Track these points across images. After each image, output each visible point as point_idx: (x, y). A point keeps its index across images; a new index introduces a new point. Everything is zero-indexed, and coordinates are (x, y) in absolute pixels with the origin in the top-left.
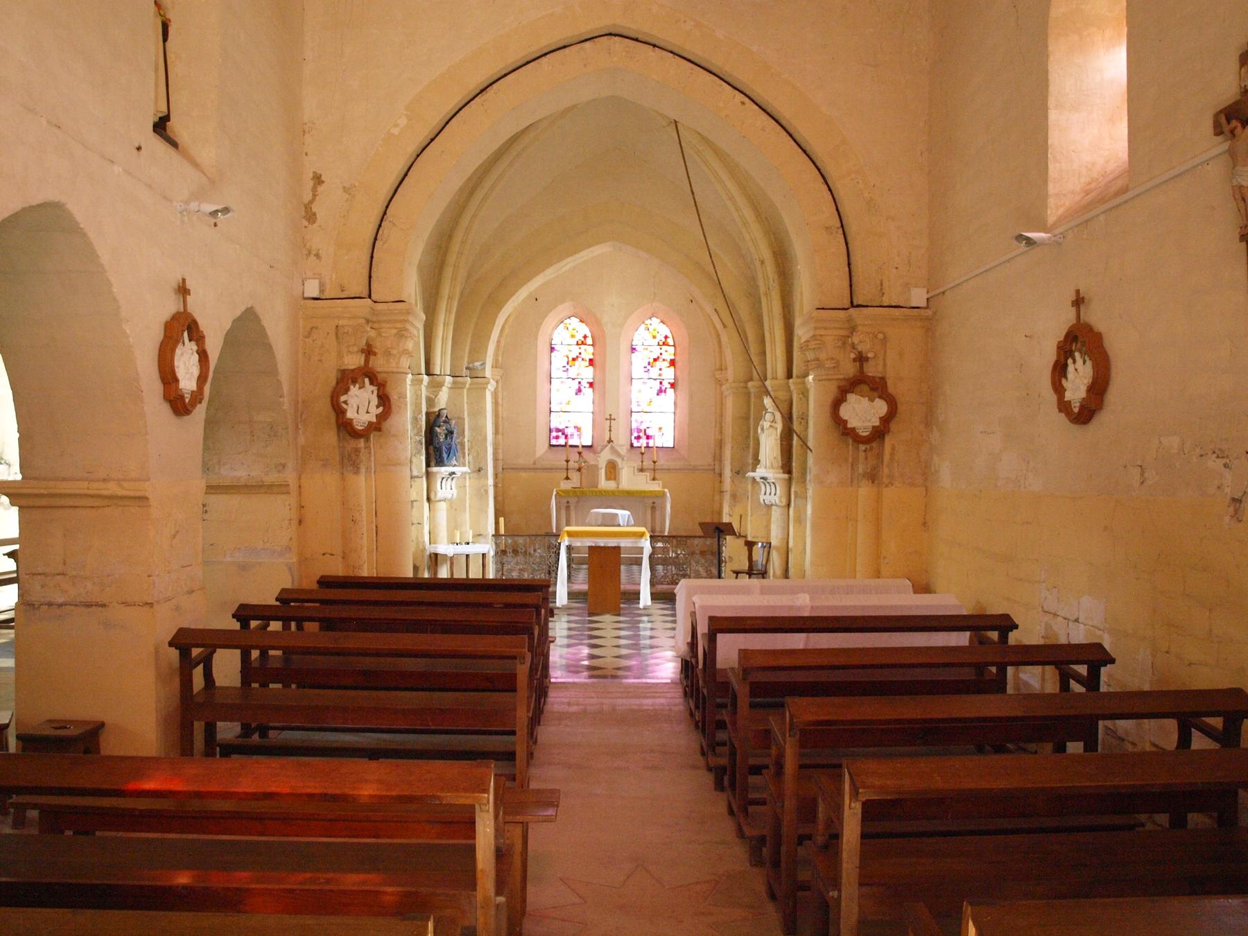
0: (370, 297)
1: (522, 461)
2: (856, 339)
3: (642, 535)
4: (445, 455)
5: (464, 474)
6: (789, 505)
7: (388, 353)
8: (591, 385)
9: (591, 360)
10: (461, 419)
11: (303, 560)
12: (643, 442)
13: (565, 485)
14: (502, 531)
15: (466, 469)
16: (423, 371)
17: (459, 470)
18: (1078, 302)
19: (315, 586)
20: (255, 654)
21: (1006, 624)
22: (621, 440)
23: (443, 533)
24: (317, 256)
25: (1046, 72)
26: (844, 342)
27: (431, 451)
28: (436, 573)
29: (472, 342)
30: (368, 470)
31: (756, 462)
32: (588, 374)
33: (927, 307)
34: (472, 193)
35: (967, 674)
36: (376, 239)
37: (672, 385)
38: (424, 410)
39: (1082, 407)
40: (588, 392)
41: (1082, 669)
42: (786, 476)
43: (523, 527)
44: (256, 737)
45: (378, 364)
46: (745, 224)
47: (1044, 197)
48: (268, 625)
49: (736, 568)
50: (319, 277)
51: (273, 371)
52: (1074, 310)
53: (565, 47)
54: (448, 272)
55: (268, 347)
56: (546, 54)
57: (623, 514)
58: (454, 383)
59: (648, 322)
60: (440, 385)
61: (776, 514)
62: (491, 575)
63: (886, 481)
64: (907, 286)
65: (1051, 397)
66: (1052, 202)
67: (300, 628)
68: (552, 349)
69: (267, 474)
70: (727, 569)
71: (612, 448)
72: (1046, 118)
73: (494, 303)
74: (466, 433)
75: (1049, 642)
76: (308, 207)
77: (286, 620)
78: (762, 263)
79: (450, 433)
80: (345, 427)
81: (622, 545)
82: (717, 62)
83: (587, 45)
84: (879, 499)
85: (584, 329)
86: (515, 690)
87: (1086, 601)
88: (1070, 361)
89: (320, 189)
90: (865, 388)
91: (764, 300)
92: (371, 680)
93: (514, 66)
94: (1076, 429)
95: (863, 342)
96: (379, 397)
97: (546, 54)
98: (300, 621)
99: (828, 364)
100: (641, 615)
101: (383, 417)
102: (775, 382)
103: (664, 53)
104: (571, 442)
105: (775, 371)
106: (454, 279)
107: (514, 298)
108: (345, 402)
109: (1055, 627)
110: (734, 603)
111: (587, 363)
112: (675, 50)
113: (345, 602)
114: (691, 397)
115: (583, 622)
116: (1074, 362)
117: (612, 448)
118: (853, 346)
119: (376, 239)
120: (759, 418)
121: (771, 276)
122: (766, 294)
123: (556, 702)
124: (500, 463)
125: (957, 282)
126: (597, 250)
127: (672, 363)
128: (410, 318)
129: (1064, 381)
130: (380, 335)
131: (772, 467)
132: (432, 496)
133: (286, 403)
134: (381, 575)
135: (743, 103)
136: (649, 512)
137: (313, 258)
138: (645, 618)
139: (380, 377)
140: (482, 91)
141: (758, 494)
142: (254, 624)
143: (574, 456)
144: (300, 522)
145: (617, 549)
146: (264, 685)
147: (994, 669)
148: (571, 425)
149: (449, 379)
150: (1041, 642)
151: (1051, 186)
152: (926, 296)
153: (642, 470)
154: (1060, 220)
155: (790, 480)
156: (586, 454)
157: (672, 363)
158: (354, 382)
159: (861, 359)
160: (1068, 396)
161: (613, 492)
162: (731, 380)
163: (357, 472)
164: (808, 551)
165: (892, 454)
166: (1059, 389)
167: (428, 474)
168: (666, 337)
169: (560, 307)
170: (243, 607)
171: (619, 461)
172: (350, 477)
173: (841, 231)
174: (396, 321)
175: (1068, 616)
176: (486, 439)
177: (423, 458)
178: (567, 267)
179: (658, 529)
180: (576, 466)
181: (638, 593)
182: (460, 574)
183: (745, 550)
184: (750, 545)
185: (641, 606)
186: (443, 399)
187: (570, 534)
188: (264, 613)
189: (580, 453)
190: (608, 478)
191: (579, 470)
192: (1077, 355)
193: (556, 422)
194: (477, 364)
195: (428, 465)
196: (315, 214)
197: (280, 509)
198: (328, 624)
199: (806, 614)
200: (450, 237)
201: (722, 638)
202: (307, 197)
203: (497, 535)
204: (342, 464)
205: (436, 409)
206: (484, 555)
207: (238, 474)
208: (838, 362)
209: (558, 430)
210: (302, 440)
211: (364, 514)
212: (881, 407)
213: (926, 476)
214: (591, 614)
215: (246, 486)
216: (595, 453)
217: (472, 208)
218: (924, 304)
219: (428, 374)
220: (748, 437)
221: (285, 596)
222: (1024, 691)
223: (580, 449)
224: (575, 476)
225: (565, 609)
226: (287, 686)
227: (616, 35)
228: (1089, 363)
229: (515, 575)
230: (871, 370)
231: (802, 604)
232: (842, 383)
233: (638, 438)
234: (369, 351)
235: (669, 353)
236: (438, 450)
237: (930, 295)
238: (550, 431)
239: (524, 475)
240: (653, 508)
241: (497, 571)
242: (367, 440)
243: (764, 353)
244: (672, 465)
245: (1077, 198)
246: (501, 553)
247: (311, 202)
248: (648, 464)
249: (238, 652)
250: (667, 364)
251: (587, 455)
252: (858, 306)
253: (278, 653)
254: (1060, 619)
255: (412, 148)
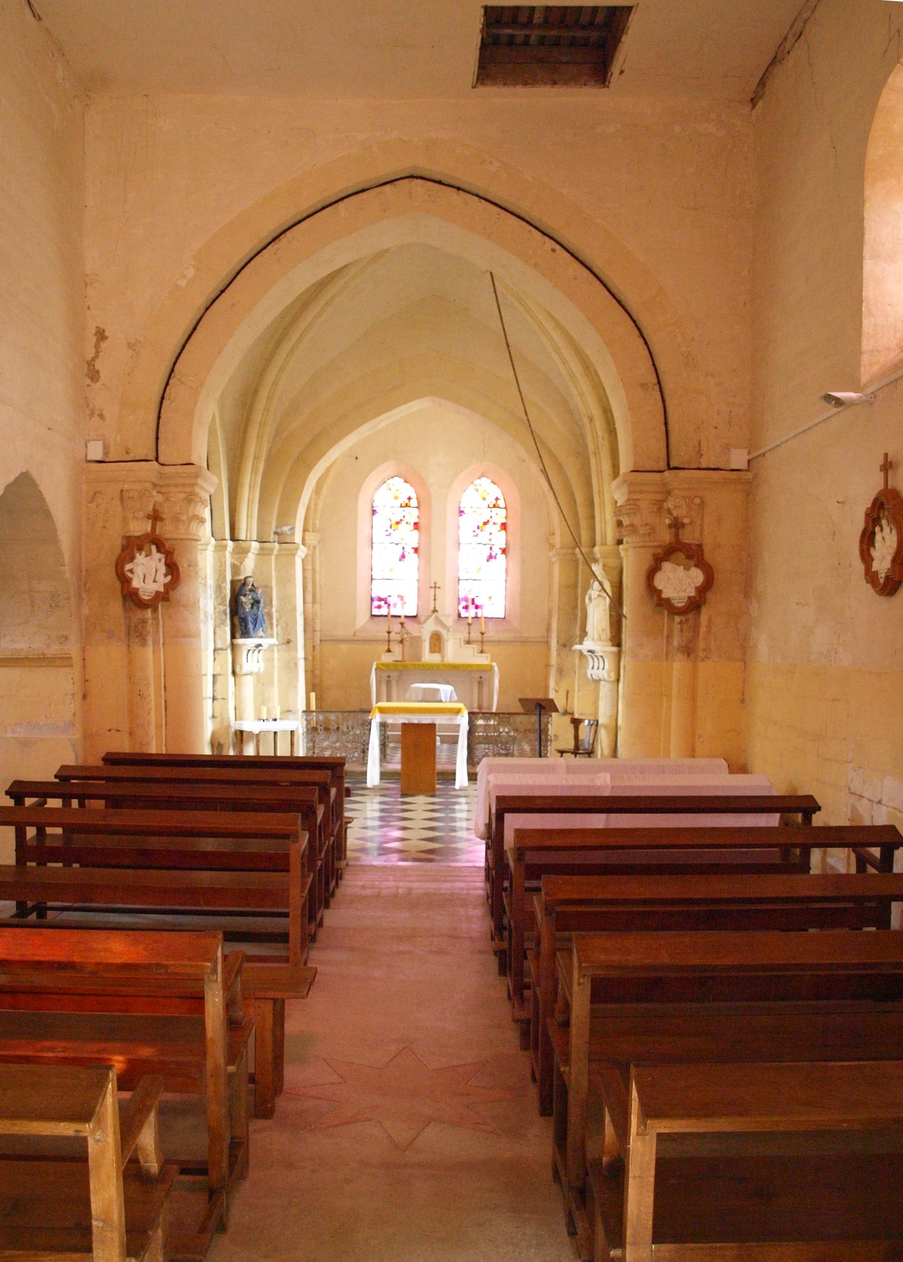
0: (157, 459)
1: (341, 633)
2: (669, 504)
3: (458, 711)
4: (251, 626)
5: (271, 646)
6: (618, 680)
7: (177, 519)
8: (416, 550)
9: (416, 524)
10: (268, 587)
11: (88, 736)
12: (472, 612)
13: (387, 659)
14: (313, 707)
15: (274, 641)
16: (228, 536)
17: (266, 642)
18: (887, 466)
19: (101, 763)
20: (31, 832)
21: (809, 806)
22: (448, 609)
23: (249, 708)
24: (101, 416)
25: (862, 220)
26: (659, 507)
27: (237, 621)
28: (241, 751)
29: (281, 505)
30: (156, 642)
31: (584, 633)
32: (412, 538)
33: (748, 470)
34: (279, 343)
35: (774, 856)
36: (163, 398)
37: (504, 551)
38: (229, 578)
39: (887, 578)
40: (412, 557)
41: (876, 852)
42: (615, 649)
43: (336, 703)
44: (33, 917)
45: (166, 530)
46: (572, 377)
47: (858, 352)
48: (45, 803)
49: (561, 748)
50: (102, 438)
51: (52, 537)
52: (882, 474)
53: (363, 191)
54: (254, 431)
55: (47, 514)
56: (342, 199)
57: (446, 690)
58: (261, 549)
59: (477, 482)
60: (246, 551)
61: (605, 690)
62: (301, 751)
63: (701, 654)
64: (727, 448)
65: (860, 567)
66: (865, 359)
67: (82, 805)
68: (374, 512)
69: (48, 646)
70: (552, 748)
71: (437, 618)
72: (862, 268)
73: (304, 463)
74: (275, 602)
75: (854, 824)
76: (90, 364)
77: (66, 798)
78: (591, 419)
79: (256, 602)
80: (131, 597)
81: (437, 722)
82: (524, 207)
83: (387, 188)
84: (694, 674)
85: (408, 490)
86: (288, 871)
87: (889, 782)
88: (877, 529)
89: (104, 345)
90: (681, 556)
91: (593, 461)
92: (146, 860)
93: (310, 212)
94: (883, 600)
95: (676, 506)
96: (167, 565)
97: (342, 199)
98: (82, 798)
99: (642, 531)
100: (458, 796)
101: (651, 574)
102: (605, 548)
103: (469, 196)
104: (394, 612)
105: (604, 537)
106: (260, 437)
107: (324, 458)
108: (131, 571)
109: (860, 810)
110: (544, 783)
111: (412, 526)
112: (481, 194)
113: (157, 781)
114: (523, 562)
115: (396, 803)
116: (882, 530)
117: (437, 618)
118: (669, 511)
119: (163, 398)
120: (587, 587)
121: (600, 433)
122: (595, 453)
123: (352, 884)
124: (318, 636)
125: (774, 444)
126: (415, 406)
127: (504, 526)
128: (200, 481)
129: (872, 549)
130: (167, 499)
131: (600, 639)
132: (238, 670)
133: (68, 572)
134: (171, 752)
135: (553, 250)
136: (476, 690)
137: (96, 418)
138: (463, 800)
139: (167, 545)
140: (274, 239)
141: (586, 668)
142: (29, 801)
143: (396, 627)
144: (85, 697)
145: (432, 727)
146: (41, 863)
147: (798, 851)
148: (395, 594)
149: (255, 545)
150: (847, 824)
151: (864, 342)
152: (747, 458)
153: (468, 642)
154: (871, 381)
155: (619, 655)
156: (409, 625)
157: (504, 526)
158: (140, 549)
159: (677, 525)
160: (875, 566)
161: (437, 666)
162: (558, 545)
163: (144, 643)
164: (621, 727)
165: (709, 626)
166: (866, 558)
167: (233, 646)
168: (497, 499)
169: (383, 467)
170: (17, 783)
171: (444, 632)
172: (136, 648)
173: (657, 388)
174: (184, 485)
175: (871, 797)
176: (294, 609)
177: (228, 629)
178: (383, 424)
179: (485, 705)
180: (399, 638)
181: (454, 774)
182: (267, 751)
183: (571, 728)
184: (576, 723)
185: (457, 786)
186: (249, 566)
187: (382, 711)
188: (42, 791)
189: (402, 624)
190: (432, 651)
191: (401, 642)
192: (884, 522)
193: (378, 590)
194: (286, 529)
195: (233, 637)
196: (98, 372)
197: (64, 682)
198: (114, 802)
199: (606, 793)
200: (256, 392)
201: (508, 817)
202: (90, 354)
203: (307, 712)
204: (128, 634)
205: (242, 577)
206: (292, 732)
207: (19, 646)
208: (653, 528)
209: (380, 599)
210: (86, 611)
211: (152, 688)
212: (697, 576)
213: (743, 651)
214: (404, 795)
215: (27, 659)
216: (419, 623)
217: (278, 361)
218: (743, 465)
219: (233, 539)
220: (575, 607)
221: (65, 773)
222: (829, 872)
223: (403, 620)
224: (397, 649)
225: (373, 789)
226: (68, 864)
227: (417, 177)
228: (894, 532)
229: (327, 754)
230: (688, 537)
231: (602, 782)
232: (659, 551)
233: (466, 608)
234: (155, 517)
235: (500, 516)
236: (244, 621)
237: (750, 457)
238: (372, 600)
239: (344, 647)
240: (480, 683)
241: (308, 749)
242: (155, 610)
243: (592, 517)
244: (502, 636)
245: (893, 355)
246: (312, 731)
247: (93, 359)
248: (475, 635)
249: (13, 828)
250: (498, 527)
251: (410, 626)
252: (675, 468)
253: (59, 831)
254: (865, 801)
255: (201, 300)
